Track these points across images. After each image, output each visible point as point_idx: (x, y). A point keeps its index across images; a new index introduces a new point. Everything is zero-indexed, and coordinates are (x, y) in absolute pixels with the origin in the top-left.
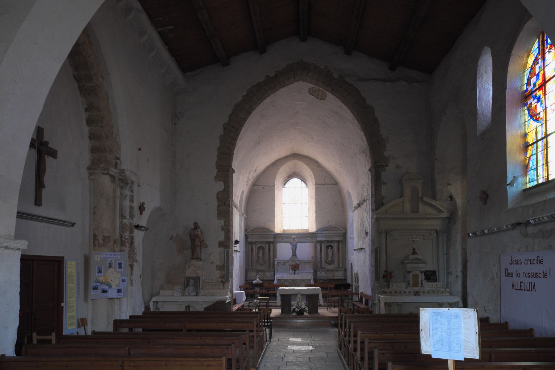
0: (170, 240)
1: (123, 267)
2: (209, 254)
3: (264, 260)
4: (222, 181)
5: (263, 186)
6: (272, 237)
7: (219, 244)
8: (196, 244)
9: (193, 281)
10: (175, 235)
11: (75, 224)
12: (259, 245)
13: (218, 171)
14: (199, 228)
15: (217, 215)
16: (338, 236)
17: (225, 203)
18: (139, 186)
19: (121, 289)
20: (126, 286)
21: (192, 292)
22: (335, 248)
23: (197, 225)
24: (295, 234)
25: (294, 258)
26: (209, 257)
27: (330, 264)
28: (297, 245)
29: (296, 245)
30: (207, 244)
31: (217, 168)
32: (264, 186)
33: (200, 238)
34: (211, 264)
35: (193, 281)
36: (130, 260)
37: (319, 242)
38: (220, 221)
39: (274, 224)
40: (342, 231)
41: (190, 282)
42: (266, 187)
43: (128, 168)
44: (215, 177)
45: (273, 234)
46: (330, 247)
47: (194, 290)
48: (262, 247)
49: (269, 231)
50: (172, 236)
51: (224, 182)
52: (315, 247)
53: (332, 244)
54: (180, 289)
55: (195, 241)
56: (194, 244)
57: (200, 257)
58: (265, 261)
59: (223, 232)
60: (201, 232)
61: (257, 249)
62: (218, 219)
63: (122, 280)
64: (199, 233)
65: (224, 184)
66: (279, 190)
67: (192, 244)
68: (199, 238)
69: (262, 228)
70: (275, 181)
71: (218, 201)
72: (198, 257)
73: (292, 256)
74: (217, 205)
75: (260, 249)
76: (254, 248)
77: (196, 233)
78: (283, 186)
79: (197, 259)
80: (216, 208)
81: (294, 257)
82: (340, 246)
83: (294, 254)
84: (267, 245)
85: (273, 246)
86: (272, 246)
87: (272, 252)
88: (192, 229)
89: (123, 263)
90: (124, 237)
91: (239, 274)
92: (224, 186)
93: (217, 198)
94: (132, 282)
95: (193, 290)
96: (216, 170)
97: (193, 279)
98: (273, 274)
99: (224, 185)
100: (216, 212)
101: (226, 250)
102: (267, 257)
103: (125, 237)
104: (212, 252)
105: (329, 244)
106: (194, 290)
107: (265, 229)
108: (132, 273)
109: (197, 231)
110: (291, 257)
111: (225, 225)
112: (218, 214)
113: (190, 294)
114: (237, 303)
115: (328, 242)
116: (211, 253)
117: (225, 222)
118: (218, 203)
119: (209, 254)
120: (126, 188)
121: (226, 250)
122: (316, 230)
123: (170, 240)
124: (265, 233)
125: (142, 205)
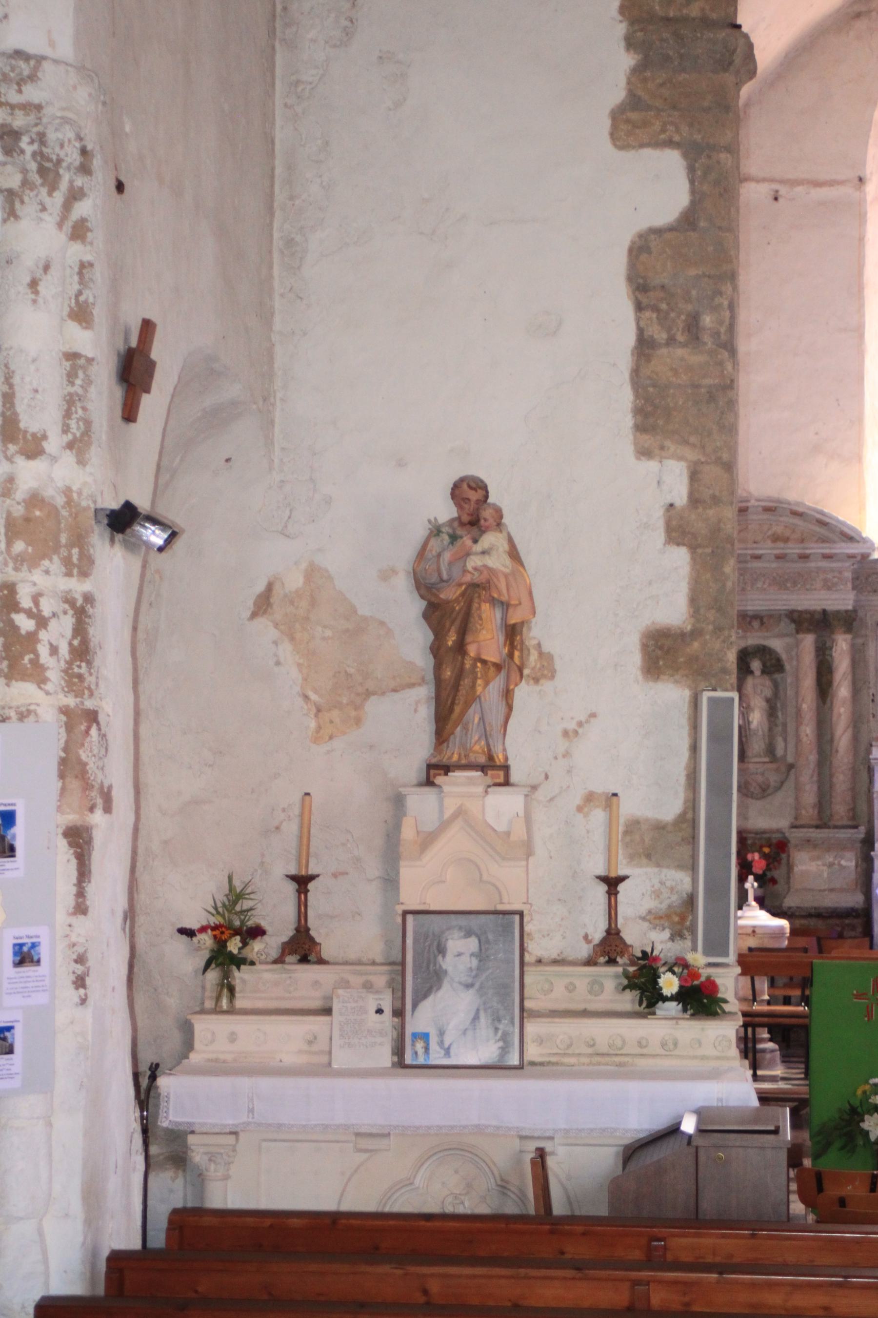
0: (254, 615)
1: (19, 845)
2: (566, 733)
3: (779, 752)
4: (670, 143)
5: (772, 180)
6: (848, 575)
7: (644, 647)
8: (472, 650)
9: (472, 944)
10: (294, 581)
13: (637, 71)
14: (499, 525)
15: (628, 421)
17: (693, 326)
18: (120, 187)
19: (9, 1029)
20: (41, 999)
21: (465, 1032)
23: (474, 496)
26: (567, 755)
30: (546, 648)
31: (630, 43)
32: (782, 182)
33: (506, 606)
34: (580, 809)
35: (472, 944)
36: (63, 789)
38: (652, 465)
41: (442, 950)
42: (800, 189)
43: (52, 44)
44: (618, 116)
45: (851, 557)
47: (483, 1019)
48: (763, 651)
49: (818, 529)
50: (270, 588)
51: (685, 156)
54: (379, 1011)
55: (463, 632)
56: (461, 647)
57: (500, 758)
58: (791, 767)
59: (680, 557)
60: (514, 554)
62: (644, 453)
63: (18, 948)
64: (499, 562)
65: (691, 170)
67: (436, 649)
68: (493, 601)
69: (767, 509)
70: (866, 143)
71: (639, 307)
72: (491, 758)
74: (630, 338)
75: (752, 672)
77: (474, 562)
79: (483, 769)
80: (625, 361)
84: (808, 641)
85: (853, 646)
86: (842, 644)
87: (843, 691)
88: (436, 531)
89: (20, 819)
90: (26, 602)
91: (138, 893)
92: (693, 192)
93: (630, 279)
94: (79, 969)
95: (476, 1018)
96: (626, 61)
97: (469, 933)
99: (692, 182)
100: (626, 397)
101: (710, 700)
102: (808, 731)
103: (36, 602)
104: (593, 715)
106: (483, 1019)
107: (795, 513)
108: (81, 894)
109: (478, 548)
111: (694, 500)
112: (638, 411)
113: (447, 1052)
116: (580, 724)
117: (694, 476)
118: (638, 320)
119: (566, 733)
120: (44, 209)
121: (710, 700)
123: (254, 615)
124: (793, 550)
125: (134, 344)
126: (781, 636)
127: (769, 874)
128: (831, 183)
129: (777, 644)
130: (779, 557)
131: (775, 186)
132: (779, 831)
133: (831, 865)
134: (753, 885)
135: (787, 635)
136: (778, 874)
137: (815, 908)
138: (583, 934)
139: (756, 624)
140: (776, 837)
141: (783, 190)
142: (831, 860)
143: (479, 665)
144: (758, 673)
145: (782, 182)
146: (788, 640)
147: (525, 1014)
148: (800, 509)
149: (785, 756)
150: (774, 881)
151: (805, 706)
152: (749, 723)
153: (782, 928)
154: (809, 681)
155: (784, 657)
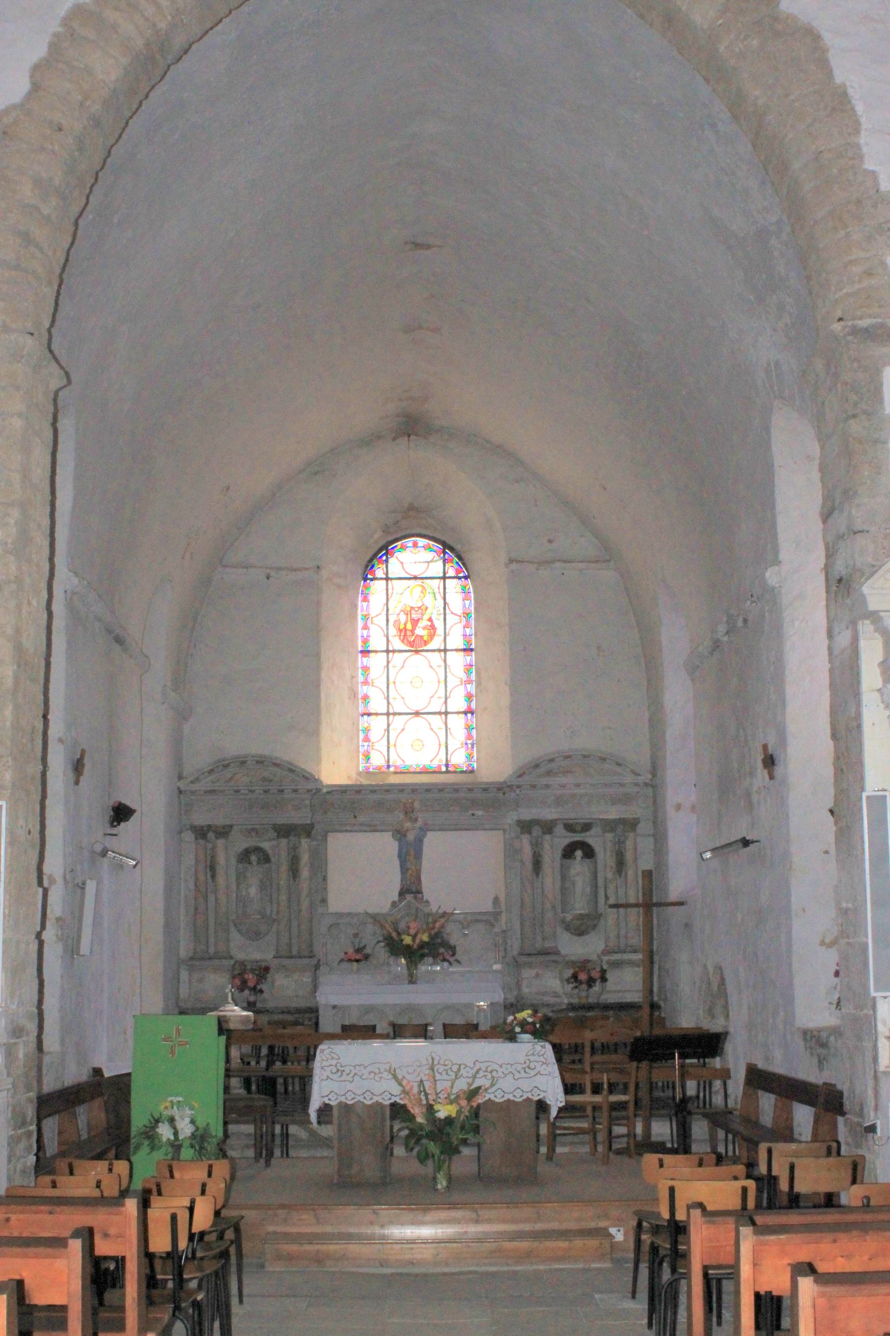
11: (823, 943)
12: (240, 843)
16: (615, 801)
22: (605, 857)
24: (414, 789)
25: (409, 905)
27: (580, 932)
28: (425, 840)
29: (419, 841)
32: (272, 568)
37: (525, 826)
39: (318, 742)
40: (639, 775)
46: (579, 853)
48: (258, 849)
52: (511, 852)
53: (592, 838)
61: (233, 861)
66: (339, 587)
73: (402, 894)
75: (250, 863)
76: (221, 859)
78: (360, 570)
81: (409, 897)
82: (629, 844)
83: (636, 905)
98: (307, 979)
105: (578, 837)
110: (396, 898)
114: (15, 1283)
115: (570, 827)
122: (511, 772)
126: (270, 840)
127: (259, 987)
128: (300, 570)
129: (266, 845)
130: (266, 792)
131: (268, 571)
132: (265, 961)
133: (296, 981)
134: (231, 991)
135: (274, 839)
136: (264, 987)
137: (287, 1008)
138: (662, 1169)
139: (253, 834)
140: (264, 964)
141: (273, 574)
142: (297, 977)
143: (134, 863)
144: (255, 863)
145: (272, 568)
146: (274, 843)
147: (291, 1143)
148: (278, 762)
149: (271, 914)
150: (261, 991)
151: (282, 883)
152: (249, 894)
153: (248, 1016)
154: (284, 867)
155: (270, 852)
